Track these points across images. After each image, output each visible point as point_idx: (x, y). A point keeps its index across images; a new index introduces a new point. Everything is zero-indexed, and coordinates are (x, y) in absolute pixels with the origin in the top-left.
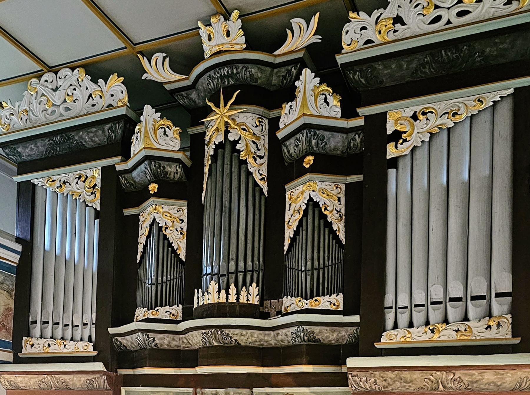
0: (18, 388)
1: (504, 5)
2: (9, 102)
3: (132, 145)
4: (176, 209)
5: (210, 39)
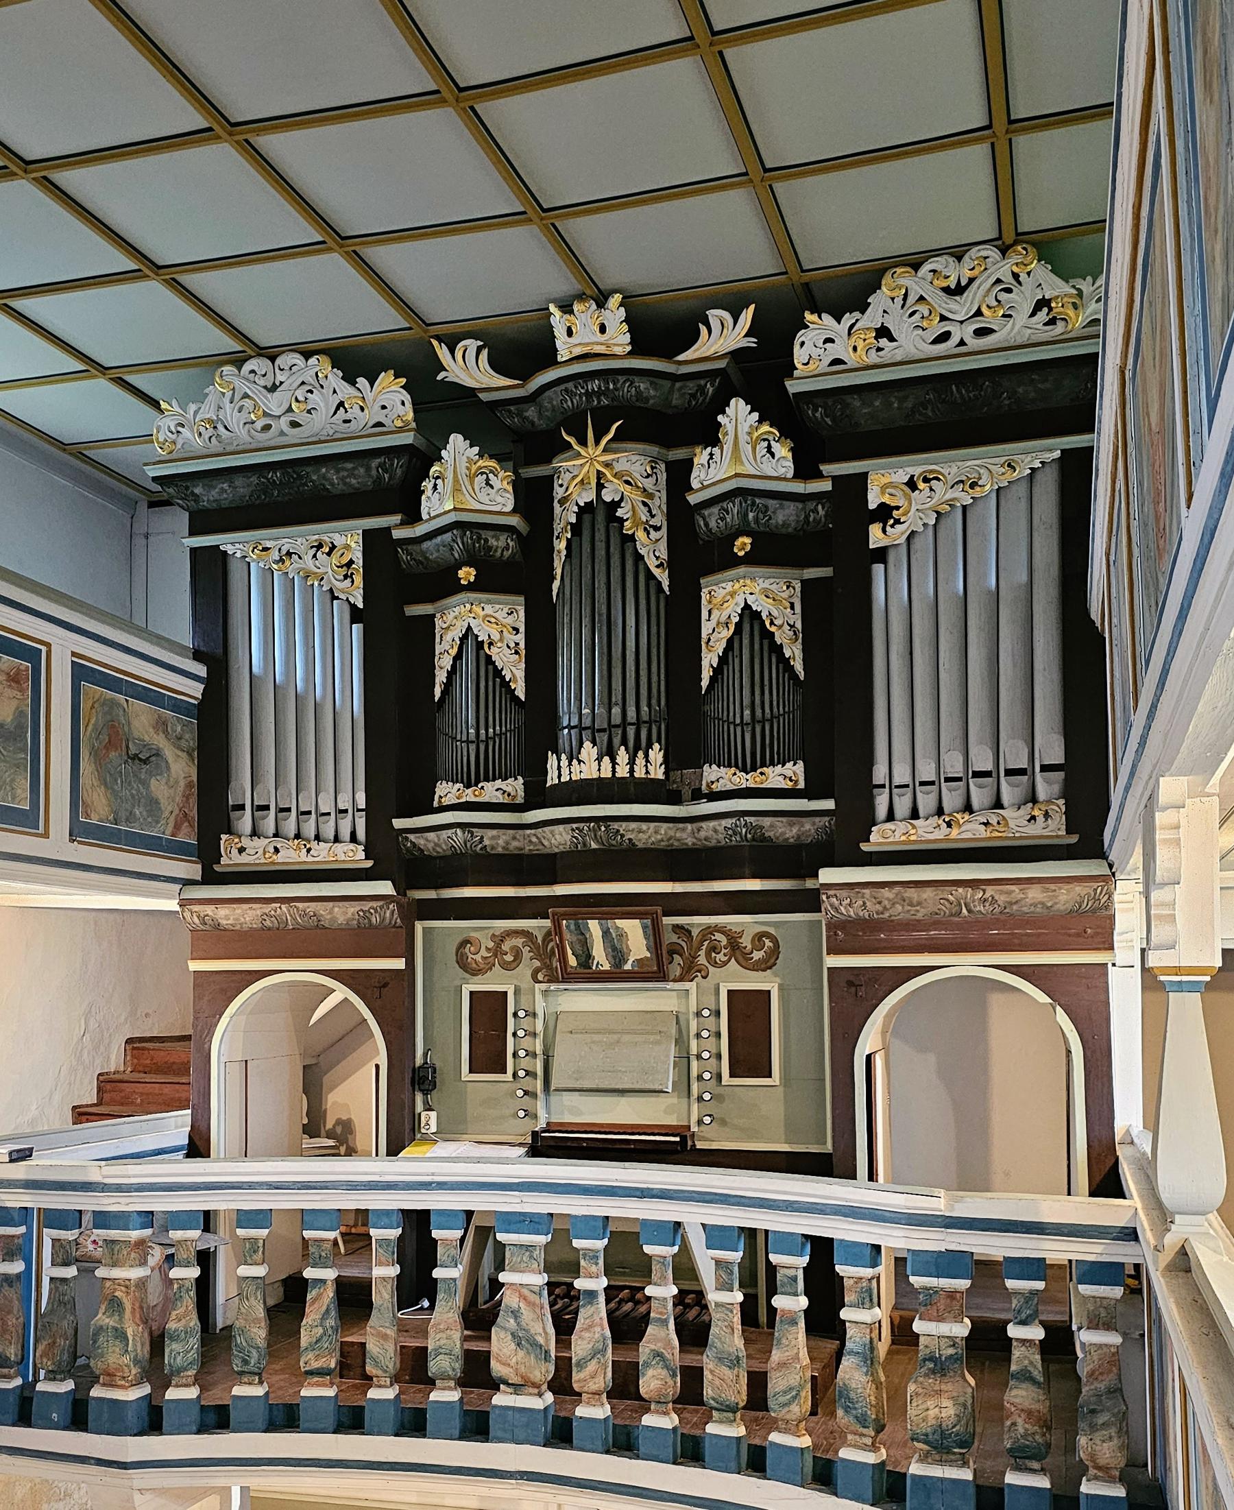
0: (217, 927)
2: (174, 402)
3: (423, 497)
4: (506, 610)
5: (570, 333)
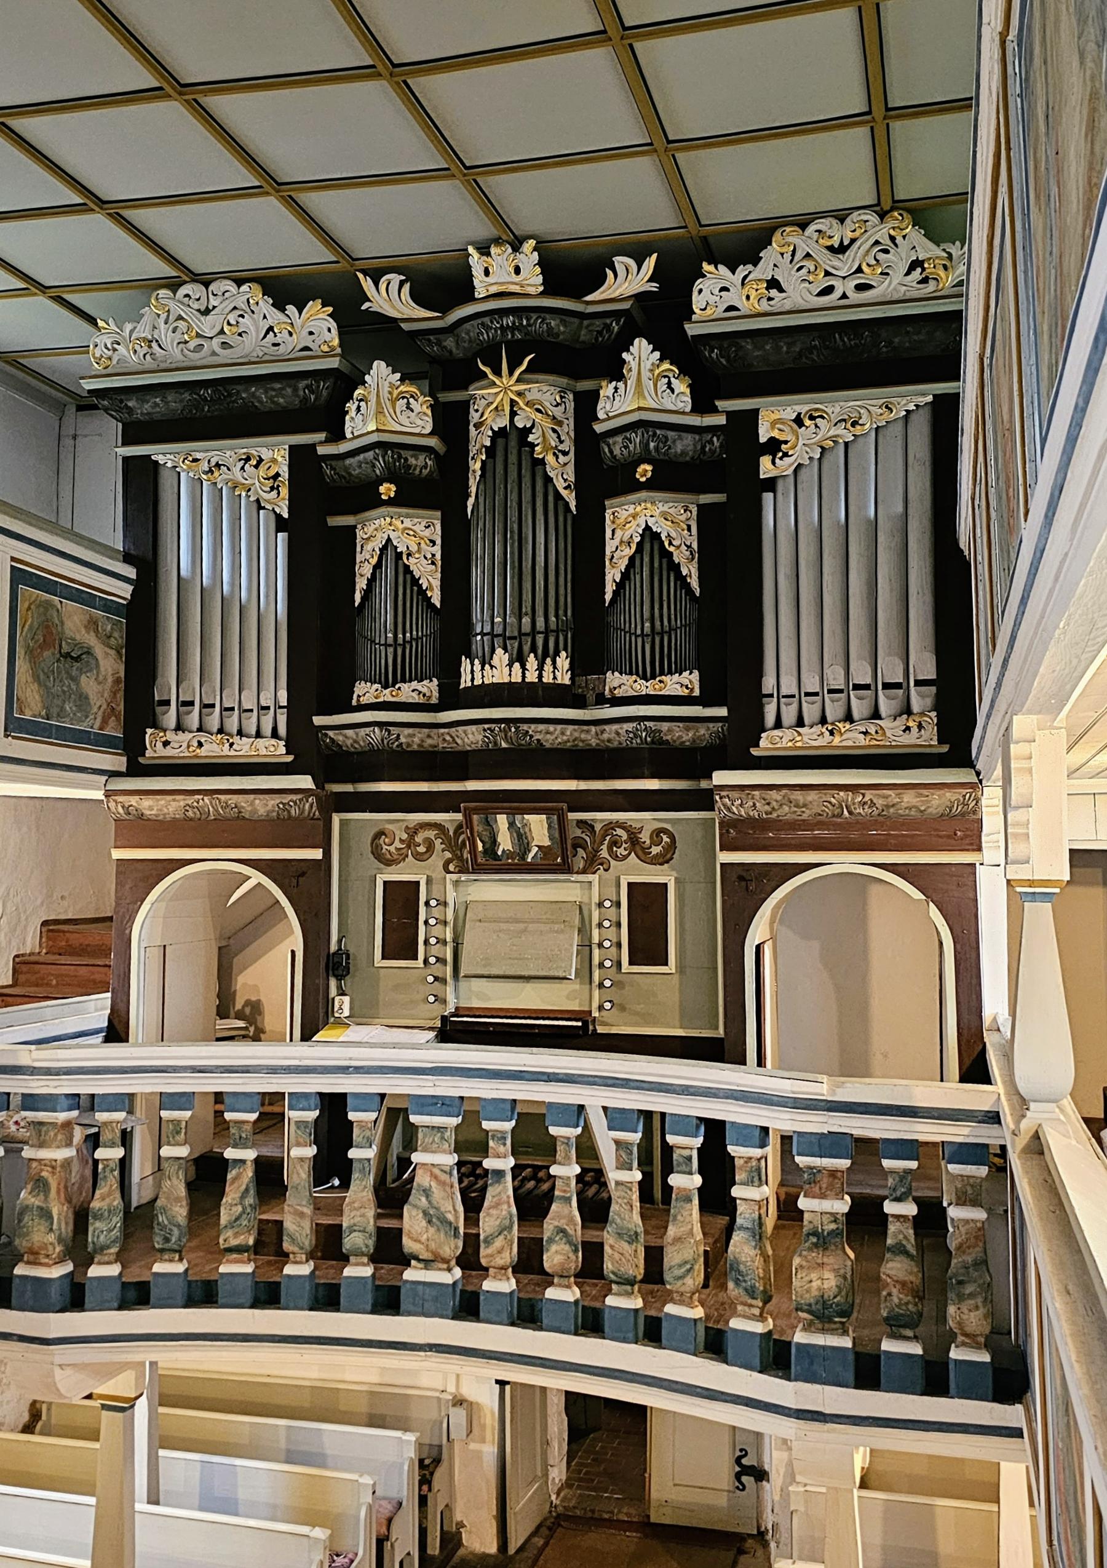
1: (918, 283)
2: (111, 321)
3: (347, 418)
4: (424, 523)
5: (487, 273)
